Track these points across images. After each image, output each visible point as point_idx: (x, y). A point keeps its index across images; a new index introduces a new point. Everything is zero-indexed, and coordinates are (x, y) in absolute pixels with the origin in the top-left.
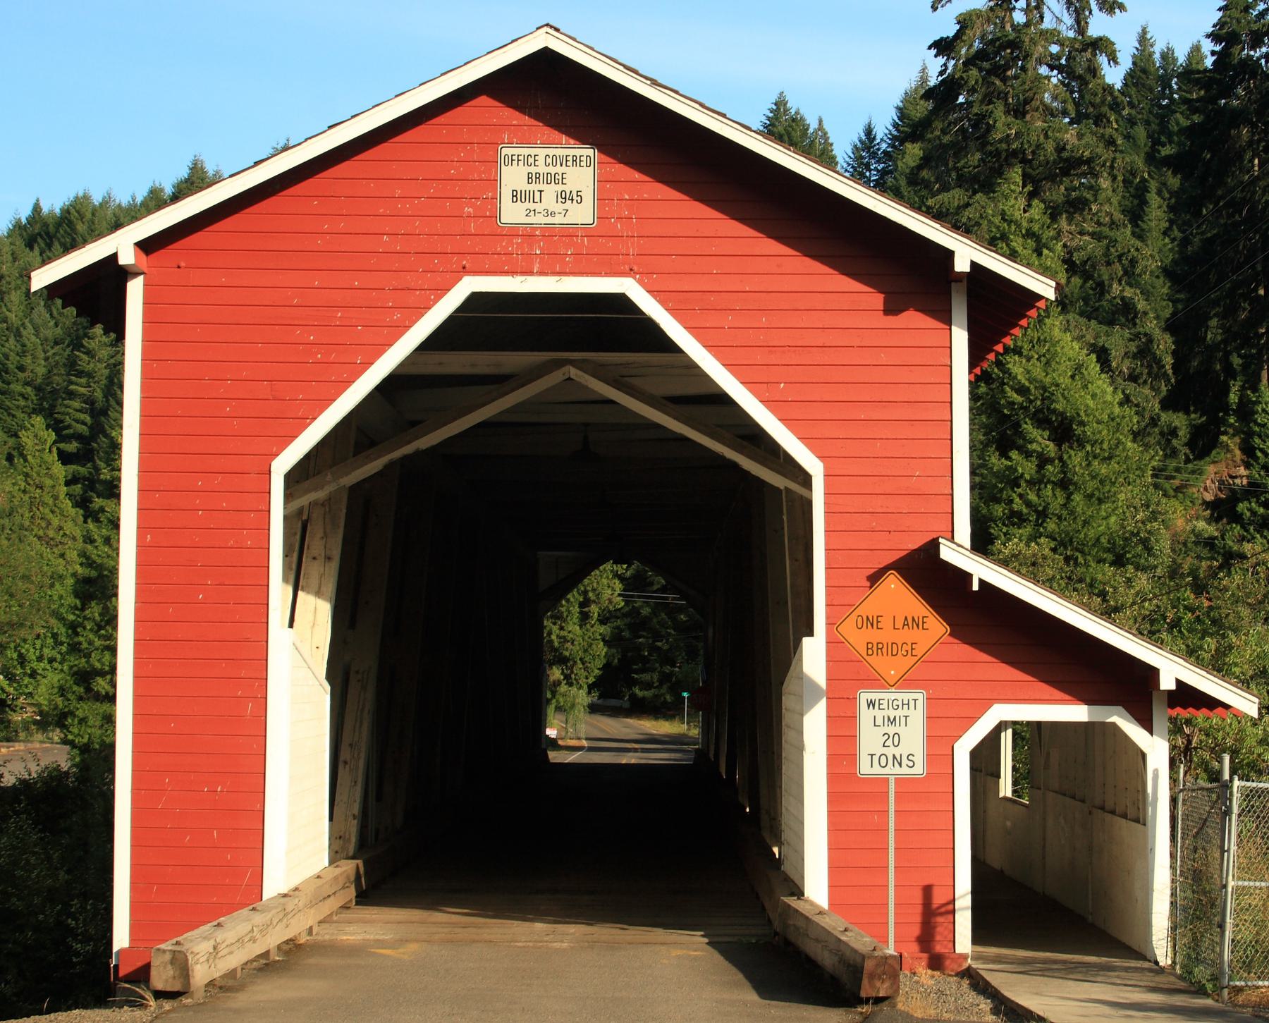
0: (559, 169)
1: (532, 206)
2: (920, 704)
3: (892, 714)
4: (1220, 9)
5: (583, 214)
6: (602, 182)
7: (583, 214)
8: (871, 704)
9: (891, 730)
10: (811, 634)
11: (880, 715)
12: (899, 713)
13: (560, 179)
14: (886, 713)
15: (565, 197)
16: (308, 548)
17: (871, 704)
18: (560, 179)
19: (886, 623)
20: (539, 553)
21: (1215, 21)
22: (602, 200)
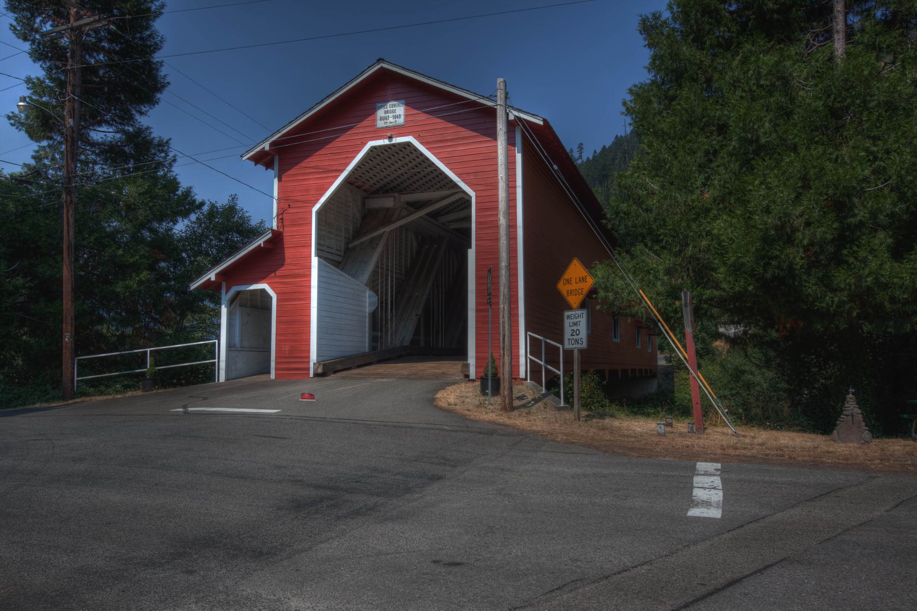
0: (394, 108)
1: (386, 121)
2: (585, 316)
3: (575, 320)
4: (168, 83)
5: (401, 121)
6: (406, 110)
7: (401, 121)
8: (568, 317)
9: (575, 328)
10: (471, 248)
11: (571, 321)
12: (577, 320)
13: (394, 111)
14: (573, 320)
15: (395, 117)
16: (325, 265)
17: (568, 317)
18: (394, 111)
19: (573, 281)
20: (699, 463)
21: (647, 61)
22: (406, 116)
